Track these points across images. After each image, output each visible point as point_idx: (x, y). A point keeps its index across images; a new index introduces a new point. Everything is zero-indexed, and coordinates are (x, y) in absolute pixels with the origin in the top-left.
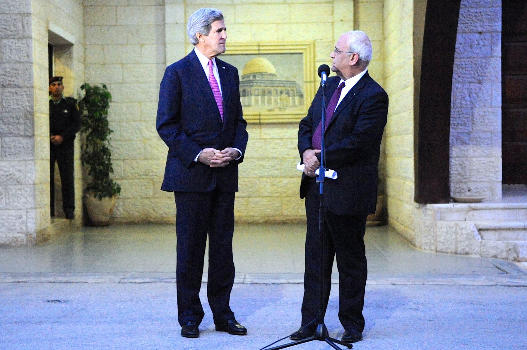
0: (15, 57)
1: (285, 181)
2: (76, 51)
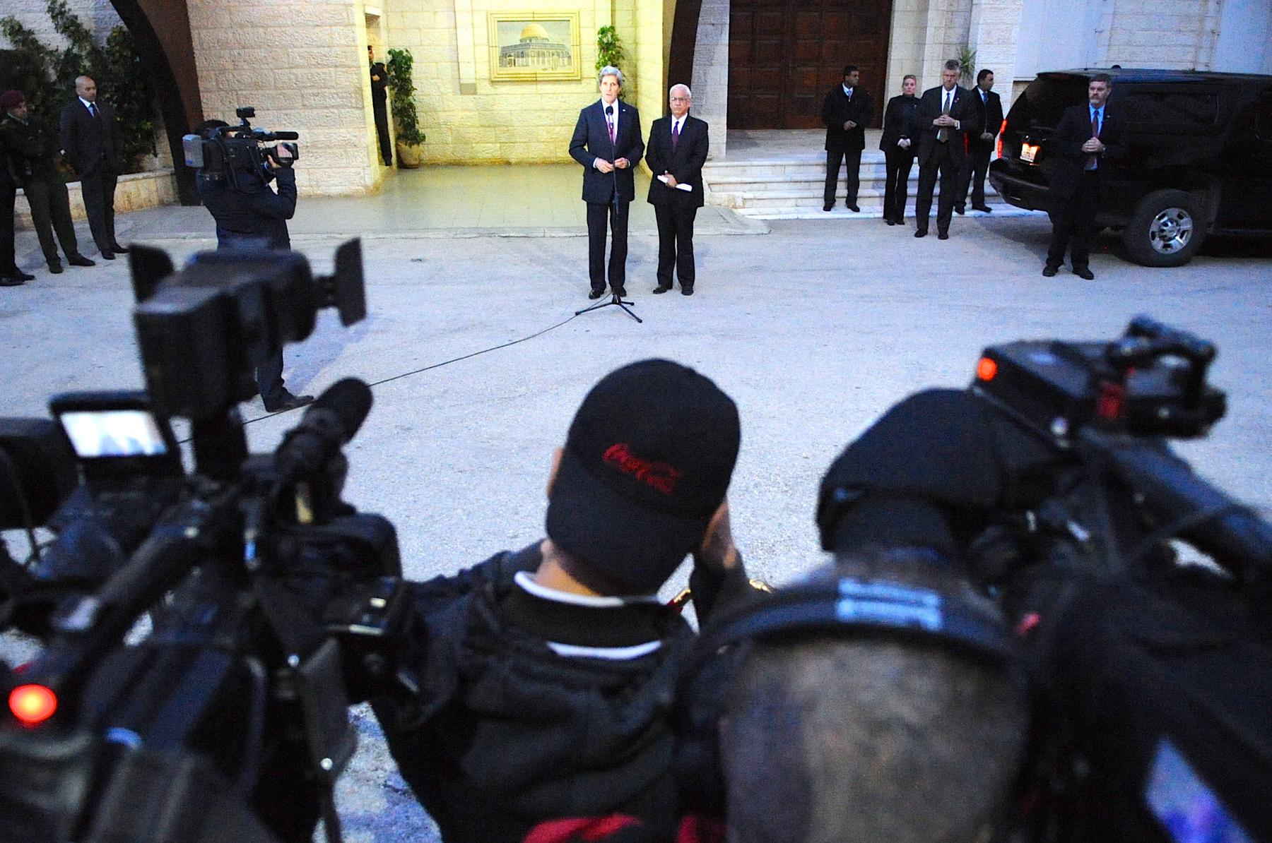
0: (343, 42)
1: (558, 129)
2: (382, 21)
